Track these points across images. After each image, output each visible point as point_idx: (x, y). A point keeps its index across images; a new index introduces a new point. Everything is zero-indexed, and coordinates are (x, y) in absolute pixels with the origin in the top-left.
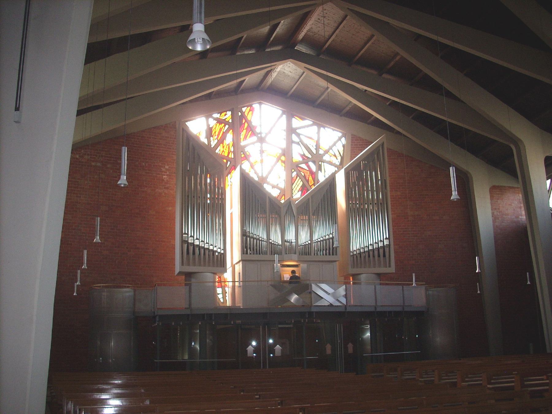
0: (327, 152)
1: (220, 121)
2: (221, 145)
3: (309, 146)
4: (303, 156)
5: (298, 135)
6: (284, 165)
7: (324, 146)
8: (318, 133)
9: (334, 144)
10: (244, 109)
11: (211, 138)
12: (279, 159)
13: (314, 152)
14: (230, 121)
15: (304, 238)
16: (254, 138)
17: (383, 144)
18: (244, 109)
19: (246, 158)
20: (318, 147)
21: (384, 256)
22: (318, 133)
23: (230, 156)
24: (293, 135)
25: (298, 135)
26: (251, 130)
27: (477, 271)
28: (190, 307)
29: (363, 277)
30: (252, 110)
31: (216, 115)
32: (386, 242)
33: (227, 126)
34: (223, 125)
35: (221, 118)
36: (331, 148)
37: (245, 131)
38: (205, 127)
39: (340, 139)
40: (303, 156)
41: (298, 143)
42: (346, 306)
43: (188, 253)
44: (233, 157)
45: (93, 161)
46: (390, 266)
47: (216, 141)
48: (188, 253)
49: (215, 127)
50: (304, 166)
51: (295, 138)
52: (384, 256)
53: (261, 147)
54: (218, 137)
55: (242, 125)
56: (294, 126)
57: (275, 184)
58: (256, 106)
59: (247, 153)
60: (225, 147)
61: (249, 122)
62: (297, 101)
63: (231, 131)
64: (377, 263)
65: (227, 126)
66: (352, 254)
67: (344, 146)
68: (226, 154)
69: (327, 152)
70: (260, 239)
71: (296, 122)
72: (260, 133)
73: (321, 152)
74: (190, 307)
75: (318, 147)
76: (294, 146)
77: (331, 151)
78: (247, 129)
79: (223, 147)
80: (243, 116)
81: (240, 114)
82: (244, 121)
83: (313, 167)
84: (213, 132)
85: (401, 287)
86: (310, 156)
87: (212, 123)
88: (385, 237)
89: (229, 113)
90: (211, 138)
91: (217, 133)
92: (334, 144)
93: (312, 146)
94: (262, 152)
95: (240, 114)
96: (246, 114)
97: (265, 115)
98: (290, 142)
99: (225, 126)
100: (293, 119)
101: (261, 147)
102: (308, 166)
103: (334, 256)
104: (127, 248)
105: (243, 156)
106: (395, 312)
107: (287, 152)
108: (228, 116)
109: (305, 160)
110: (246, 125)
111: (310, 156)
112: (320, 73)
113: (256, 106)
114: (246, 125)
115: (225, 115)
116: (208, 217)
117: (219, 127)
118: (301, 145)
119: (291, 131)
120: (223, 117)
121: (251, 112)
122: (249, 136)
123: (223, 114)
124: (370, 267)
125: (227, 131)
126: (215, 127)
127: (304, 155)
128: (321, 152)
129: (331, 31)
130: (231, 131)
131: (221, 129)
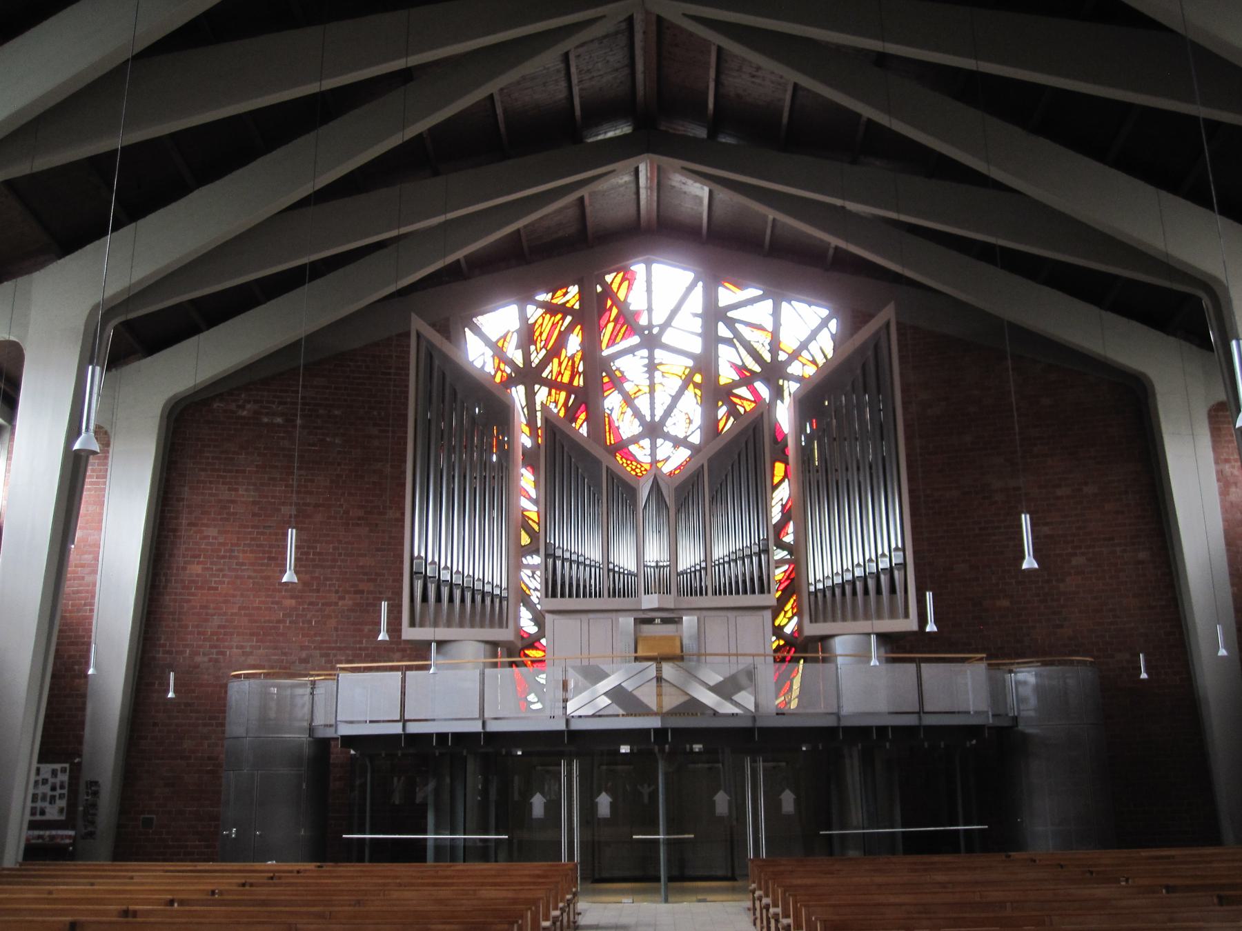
0: (795, 356)
1: (551, 309)
2: (556, 361)
3: (755, 345)
4: (741, 369)
5: (731, 323)
6: (699, 392)
7: (789, 343)
8: (776, 314)
9: (813, 335)
10: (609, 278)
11: (532, 348)
12: (688, 381)
13: (767, 357)
14: (577, 307)
15: (689, 557)
16: (635, 340)
17: (888, 325)
18: (609, 278)
19: (617, 382)
20: (775, 347)
21: (893, 590)
22: (776, 314)
23: (575, 383)
24: (721, 326)
25: (731, 323)
26: (627, 321)
27: (380, 638)
28: (921, 712)
29: (840, 645)
30: (629, 278)
31: (543, 297)
32: (897, 558)
33: (569, 319)
34: (559, 316)
35: (554, 301)
36: (804, 346)
37: (611, 326)
38: (515, 324)
39: (824, 323)
40: (741, 369)
41: (728, 342)
42: (754, 718)
43: (425, 598)
44: (581, 383)
45: (267, 414)
46: (907, 615)
47: (544, 352)
48: (425, 598)
49: (540, 321)
50: (743, 391)
51: (723, 331)
52: (893, 590)
53: (651, 357)
54: (547, 341)
55: (603, 310)
56: (723, 302)
57: (681, 436)
58: (639, 269)
59: (618, 373)
60: (563, 366)
61: (622, 306)
62: (728, 248)
63: (579, 327)
64: (478, 618)
65: (569, 319)
66: (812, 589)
67: (833, 337)
68: (566, 379)
69: (795, 356)
70: (587, 562)
71: (727, 295)
72: (650, 326)
73: (782, 357)
74: (921, 712)
75: (775, 347)
76: (723, 349)
77: (805, 353)
78: (616, 320)
79: (560, 364)
80: (608, 292)
81: (599, 289)
82: (609, 303)
83: (764, 391)
84: (537, 334)
85: (914, 665)
86: (757, 369)
87: (534, 313)
88: (893, 546)
89: (574, 290)
90: (532, 348)
91: (544, 336)
92: (813, 335)
93: (761, 342)
94: (652, 367)
95: (599, 289)
96: (615, 287)
97: (661, 287)
98: (711, 340)
99: (563, 319)
100: (721, 289)
101: (651, 357)
102: (754, 392)
103: (765, 596)
104: (337, 592)
105: (606, 380)
106: (457, 736)
107: (705, 365)
108: (571, 295)
109: (747, 378)
110: (615, 311)
111: (757, 369)
112: (728, 180)
113: (639, 269)
114: (615, 311)
115: (564, 295)
116: (491, 519)
117: (548, 321)
118: (738, 344)
119: (714, 315)
120: (559, 300)
121: (626, 284)
122: (620, 335)
123: (559, 293)
124: (855, 618)
125: (570, 328)
126: (540, 321)
127: (744, 367)
128: (782, 357)
129: (563, 84)
130: (579, 327)
131: (554, 325)
